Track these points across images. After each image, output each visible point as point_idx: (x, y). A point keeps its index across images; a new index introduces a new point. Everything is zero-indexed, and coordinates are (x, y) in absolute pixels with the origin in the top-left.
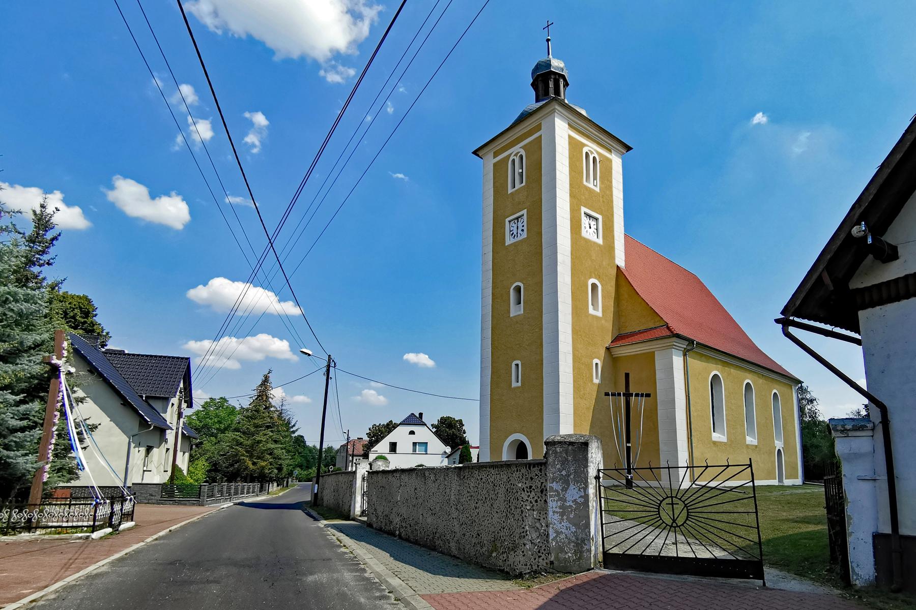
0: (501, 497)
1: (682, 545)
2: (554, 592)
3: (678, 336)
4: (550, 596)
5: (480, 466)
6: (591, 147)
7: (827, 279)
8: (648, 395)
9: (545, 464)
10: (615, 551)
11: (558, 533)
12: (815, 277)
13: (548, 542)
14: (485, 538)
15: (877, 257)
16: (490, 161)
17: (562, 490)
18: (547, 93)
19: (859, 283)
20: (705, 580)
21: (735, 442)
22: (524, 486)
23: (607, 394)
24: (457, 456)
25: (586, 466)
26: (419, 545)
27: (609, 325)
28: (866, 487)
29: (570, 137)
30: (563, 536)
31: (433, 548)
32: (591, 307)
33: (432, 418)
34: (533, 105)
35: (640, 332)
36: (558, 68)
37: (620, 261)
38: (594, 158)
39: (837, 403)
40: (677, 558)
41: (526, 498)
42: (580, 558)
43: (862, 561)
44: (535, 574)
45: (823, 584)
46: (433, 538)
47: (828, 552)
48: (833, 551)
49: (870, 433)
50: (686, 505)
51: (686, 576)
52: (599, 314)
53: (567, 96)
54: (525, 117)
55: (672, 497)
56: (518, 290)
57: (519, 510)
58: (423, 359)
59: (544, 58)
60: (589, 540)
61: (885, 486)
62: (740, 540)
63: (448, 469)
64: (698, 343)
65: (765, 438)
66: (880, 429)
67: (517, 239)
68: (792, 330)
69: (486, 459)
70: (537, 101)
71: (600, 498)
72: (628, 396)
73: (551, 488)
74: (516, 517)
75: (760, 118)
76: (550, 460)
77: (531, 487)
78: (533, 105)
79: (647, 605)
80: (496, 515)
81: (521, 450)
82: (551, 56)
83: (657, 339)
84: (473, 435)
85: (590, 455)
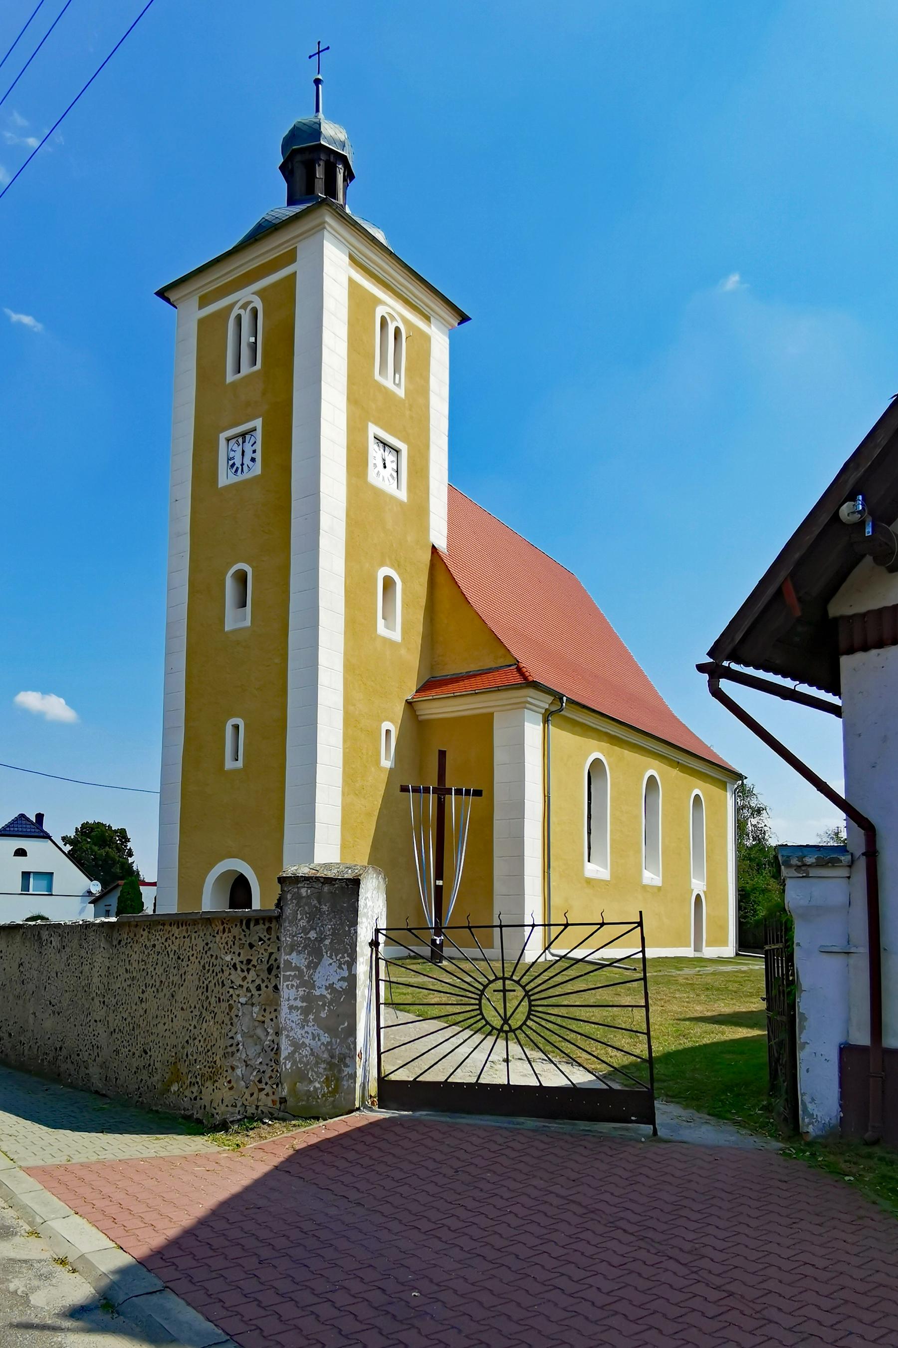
0: (192, 980)
1: (519, 1063)
2: (284, 1153)
3: (535, 685)
4: (276, 1161)
5: (158, 922)
6: (389, 306)
7: (791, 597)
8: (478, 793)
9: (278, 918)
10: (403, 1075)
11: (297, 1046)
12: (771, 590)
13: (277, 1062)
14: (158, 1056)
15: (879, 560)
16: (190, 313)
17: (308, 967)
18: (310, 189)
19: (849, 604)
20: (554, 1125)
21: (624, 881)
22: (237, 960)
23: (404, 789)
24: (113, 901)
25: (354, 923)
26: (29, 1072)
27: (412, 658)
28: (835, 963)
29: (351, 281)
30: (305, 1052)
31: (58, 1078)
32: (380, 622)
33: (63, 826)
34: (281, 209)
35: (469, 676)
36: (334, 141)
37: (439, 536)
38: (397, 331)
39: (803, 820)
40: (508, 1089)
41: (239, 982)
42: (336, 1091)
43: (820, 1091)
44: (251, 1120)
45: (754, 1131)
46: (56, 1058)
47: (765, 1075)
48: (774, 1075)
49: (844, 872)
50: (527, 992)
51: (521, 1119)
52: (396, 635)
53: (351, 197)
54: (264, 231)
55: (504, 979)
56: (241, 578)
57: (224, 1005)
58: (56, 707)
59: (306, 117)
60: (353, 1058)
61: (862, 962)
62: (619, 1054)
63: (87, 926)
64: (571, 701)
65: (676, 875)
66: (862, 864)
67: (240, 477)
68: (725, 685)
69: (171, 907)
70: (291, 202)
71: (378, 980)
72: (442, 796)
73: (288, 963)
74: (220, 1017)
75: (733, 281)
76: (288, 911)
77: (249, 961)
78: (281, 209)
79: (450, 1172)
80: (179, 1014)
81: (239, 889)
82: (321, 115)
83: (498, 689)
84: (145, 860)
85: (361, 903)
